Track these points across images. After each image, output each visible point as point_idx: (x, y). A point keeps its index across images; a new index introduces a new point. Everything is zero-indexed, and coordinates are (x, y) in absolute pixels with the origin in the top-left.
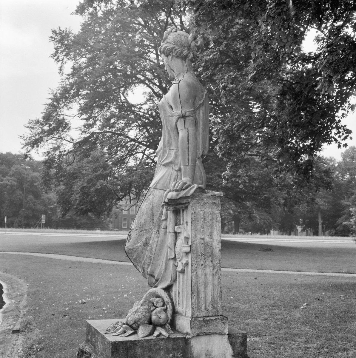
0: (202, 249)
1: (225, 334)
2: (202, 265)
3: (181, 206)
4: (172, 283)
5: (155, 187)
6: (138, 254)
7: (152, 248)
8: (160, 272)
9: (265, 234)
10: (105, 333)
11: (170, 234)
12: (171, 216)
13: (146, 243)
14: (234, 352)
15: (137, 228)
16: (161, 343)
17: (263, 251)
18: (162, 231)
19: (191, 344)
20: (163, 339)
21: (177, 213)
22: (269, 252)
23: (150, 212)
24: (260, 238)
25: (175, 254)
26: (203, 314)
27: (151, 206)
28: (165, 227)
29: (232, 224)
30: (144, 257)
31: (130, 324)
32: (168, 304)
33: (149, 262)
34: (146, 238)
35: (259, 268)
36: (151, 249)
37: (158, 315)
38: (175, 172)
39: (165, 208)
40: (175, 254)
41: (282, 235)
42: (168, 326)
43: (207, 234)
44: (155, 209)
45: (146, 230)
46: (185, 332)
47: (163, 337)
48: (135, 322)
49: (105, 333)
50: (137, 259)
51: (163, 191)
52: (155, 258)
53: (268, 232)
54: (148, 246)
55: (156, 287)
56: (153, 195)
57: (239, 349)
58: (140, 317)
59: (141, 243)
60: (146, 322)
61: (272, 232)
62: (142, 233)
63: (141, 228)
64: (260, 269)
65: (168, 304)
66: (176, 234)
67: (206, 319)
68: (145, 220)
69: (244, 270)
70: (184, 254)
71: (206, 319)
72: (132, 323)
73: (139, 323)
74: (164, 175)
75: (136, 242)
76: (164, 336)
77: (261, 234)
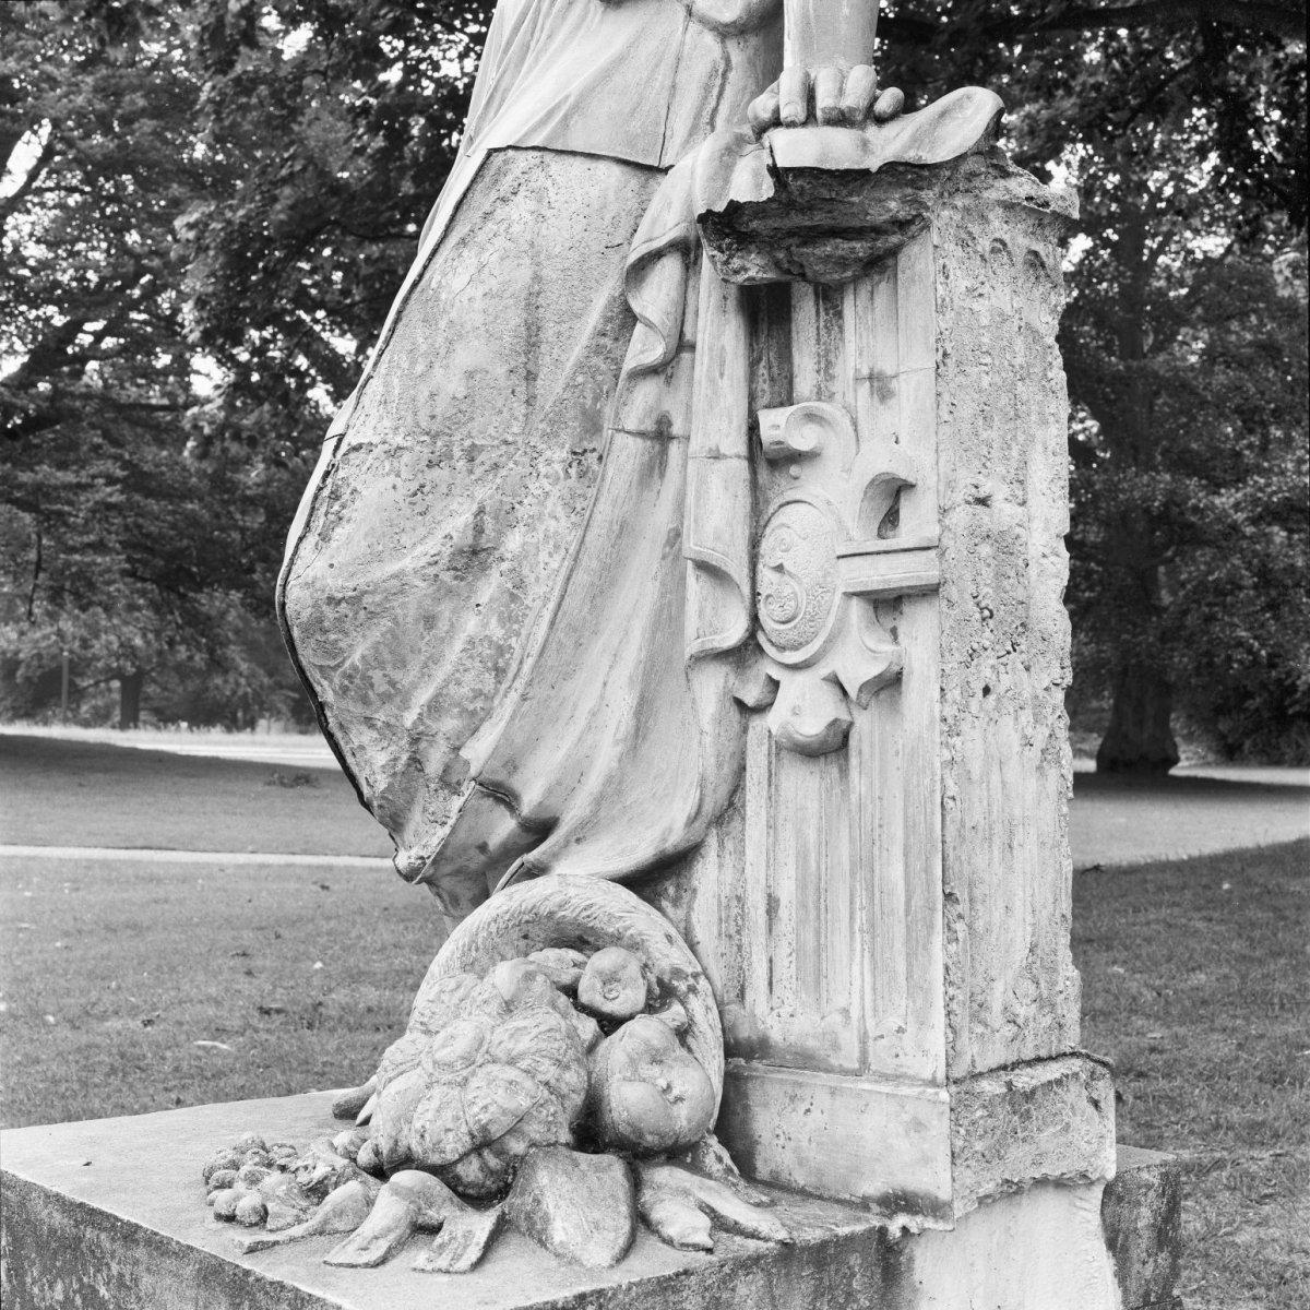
0: (987, 574)
1: (1085, 1180)
2: (986, 691)
3: (843, 247)
4: (694, 838)
5: (554, 136)
6: (394, 634)
7: (520, 585)
8: (575, 772)
9: (240, 729)
10: (251, 1250)
11: (721, 465)
12: (720, 335)
13: (475, 553)
14: (1126, 1291)
15: (399, 440)
16: (742, 1290)
17: (283, 784)
18: (627, 454)
19: (917, 1277)
20: (756, 1260)
21: (765, 311)
22: (306, 790)
23: (515, 318)
24: (227, 744)
25: (755, 619)
26: (997, 1055)
27: (524, 275)
28: (649, 426)
29: (110, 690)
30: (435, 660)
31: (435, 1159)
32: (692, 990)
33: (478, 694)
34: (481, 511)
35: (297, 849)
36: (516, 590)
37: (658, 1084)
38: (709, 39)
39: (705, 262)
40: (755, 619)
41: (302, 732)
42: (715, 1153)
43: (1001, 469)
44: (555, 300)
45: (471, 455)
46: (872, 1187)
47: (752, 1245)
48: (483, 1143)
49: (251, 1250)
50: (377, 676)
51: (612, 174)
52: (551, 659)
53: (251, 724)
54: (484, 567)
55: (534, 872)
56: (539, 195)
57: (1148, 1271)
58: (524, 1102)
59: (432, 546)
60: (565, 1136)
61: (262, 723)
62: (440, 474)
63: (435, 437)
64: (305, 852)
65: (692, 990)
66: (769, 463)
67: (1024, 1079)
68: (470, 375)
69: (242, 858)
70: (857, 608)
71: (1024, 1079)
72: (453, 1146)
73: (517, 1147)
74: (620, 60)
75: (389, 540)
76: (754, 1235)
77: (229, 730)
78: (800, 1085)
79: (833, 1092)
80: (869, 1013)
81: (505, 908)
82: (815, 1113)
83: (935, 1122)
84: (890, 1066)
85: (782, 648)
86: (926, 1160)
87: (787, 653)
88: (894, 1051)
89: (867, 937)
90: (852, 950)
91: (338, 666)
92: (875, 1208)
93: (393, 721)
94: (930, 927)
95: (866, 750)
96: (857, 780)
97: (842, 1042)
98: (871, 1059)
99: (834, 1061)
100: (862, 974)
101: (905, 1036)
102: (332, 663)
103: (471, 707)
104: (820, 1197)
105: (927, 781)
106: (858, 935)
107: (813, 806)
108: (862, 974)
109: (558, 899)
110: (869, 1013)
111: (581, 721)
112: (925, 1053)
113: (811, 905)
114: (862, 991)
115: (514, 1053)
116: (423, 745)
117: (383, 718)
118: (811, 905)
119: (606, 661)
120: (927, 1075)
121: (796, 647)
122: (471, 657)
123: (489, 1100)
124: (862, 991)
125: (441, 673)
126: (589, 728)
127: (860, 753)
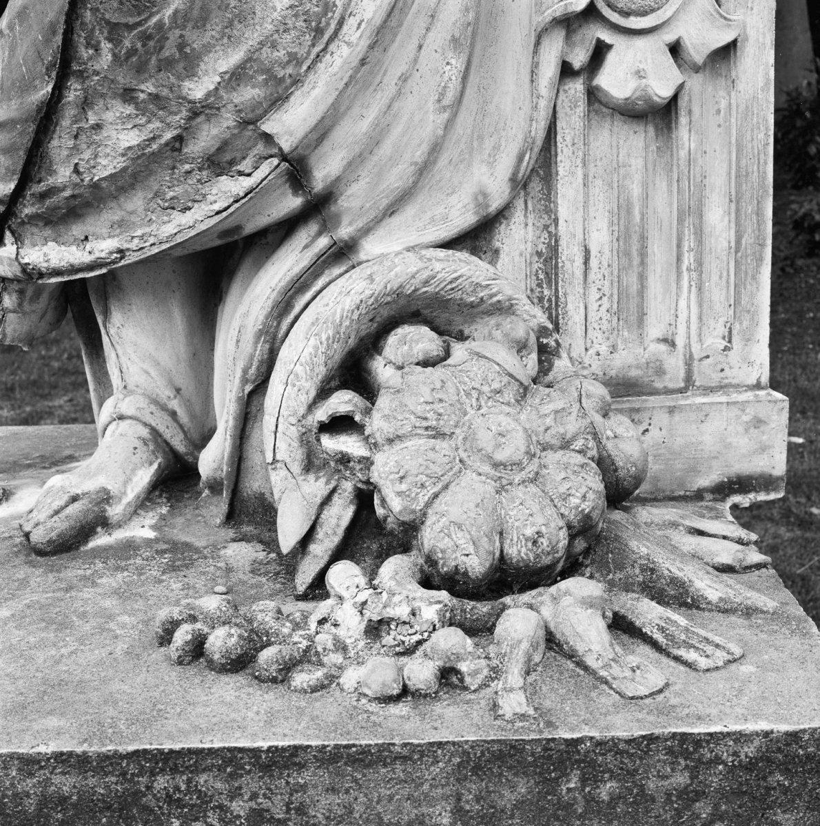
78: (638, 410)
79: (671, 410)
80: (694, 338)
81: (368, 292)
82: (654, 432)
83: (775, 417)
84: (715, 378)
85: (626, 14)
86: (763, 449)
87: (632, 18)
88: (719, 367)
89: (694, 275)
90: (679, 287)
91: (139, 24)
92: (709, 496)
93: (165, 92)
94: (760, 260)
95: (696, 110)
96: (686, 137)
97: (666, 366)
98: (696, 376)
99: (658, 385)
100: (689, 307)
101: (731, 353)
102: (131, 20)
103: (281, 74)
104: (655, 500)
105: (761, 136)
106: (685, 274)
107: (637, 163)
108: (689, 307)
109: (425, 275)
110: (694, 338)
111: (390, 88)
112: (750, 364)
113: (635, 253)
114: (688, 321)
115: (568, 436)
116: (201, 119)
117: (152, 89)
118: (635, 253)
119: (422, 22)
120: (752, 380)
121: (643, 13)
122: (296, 16)
123: (584, 490)
124: (688, 321)
125: (252, 38)
126: (399, 93)
127: (690, 112)
